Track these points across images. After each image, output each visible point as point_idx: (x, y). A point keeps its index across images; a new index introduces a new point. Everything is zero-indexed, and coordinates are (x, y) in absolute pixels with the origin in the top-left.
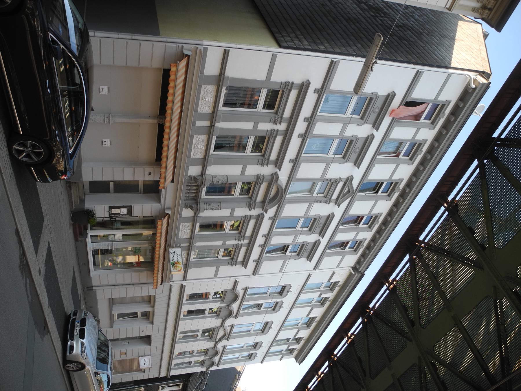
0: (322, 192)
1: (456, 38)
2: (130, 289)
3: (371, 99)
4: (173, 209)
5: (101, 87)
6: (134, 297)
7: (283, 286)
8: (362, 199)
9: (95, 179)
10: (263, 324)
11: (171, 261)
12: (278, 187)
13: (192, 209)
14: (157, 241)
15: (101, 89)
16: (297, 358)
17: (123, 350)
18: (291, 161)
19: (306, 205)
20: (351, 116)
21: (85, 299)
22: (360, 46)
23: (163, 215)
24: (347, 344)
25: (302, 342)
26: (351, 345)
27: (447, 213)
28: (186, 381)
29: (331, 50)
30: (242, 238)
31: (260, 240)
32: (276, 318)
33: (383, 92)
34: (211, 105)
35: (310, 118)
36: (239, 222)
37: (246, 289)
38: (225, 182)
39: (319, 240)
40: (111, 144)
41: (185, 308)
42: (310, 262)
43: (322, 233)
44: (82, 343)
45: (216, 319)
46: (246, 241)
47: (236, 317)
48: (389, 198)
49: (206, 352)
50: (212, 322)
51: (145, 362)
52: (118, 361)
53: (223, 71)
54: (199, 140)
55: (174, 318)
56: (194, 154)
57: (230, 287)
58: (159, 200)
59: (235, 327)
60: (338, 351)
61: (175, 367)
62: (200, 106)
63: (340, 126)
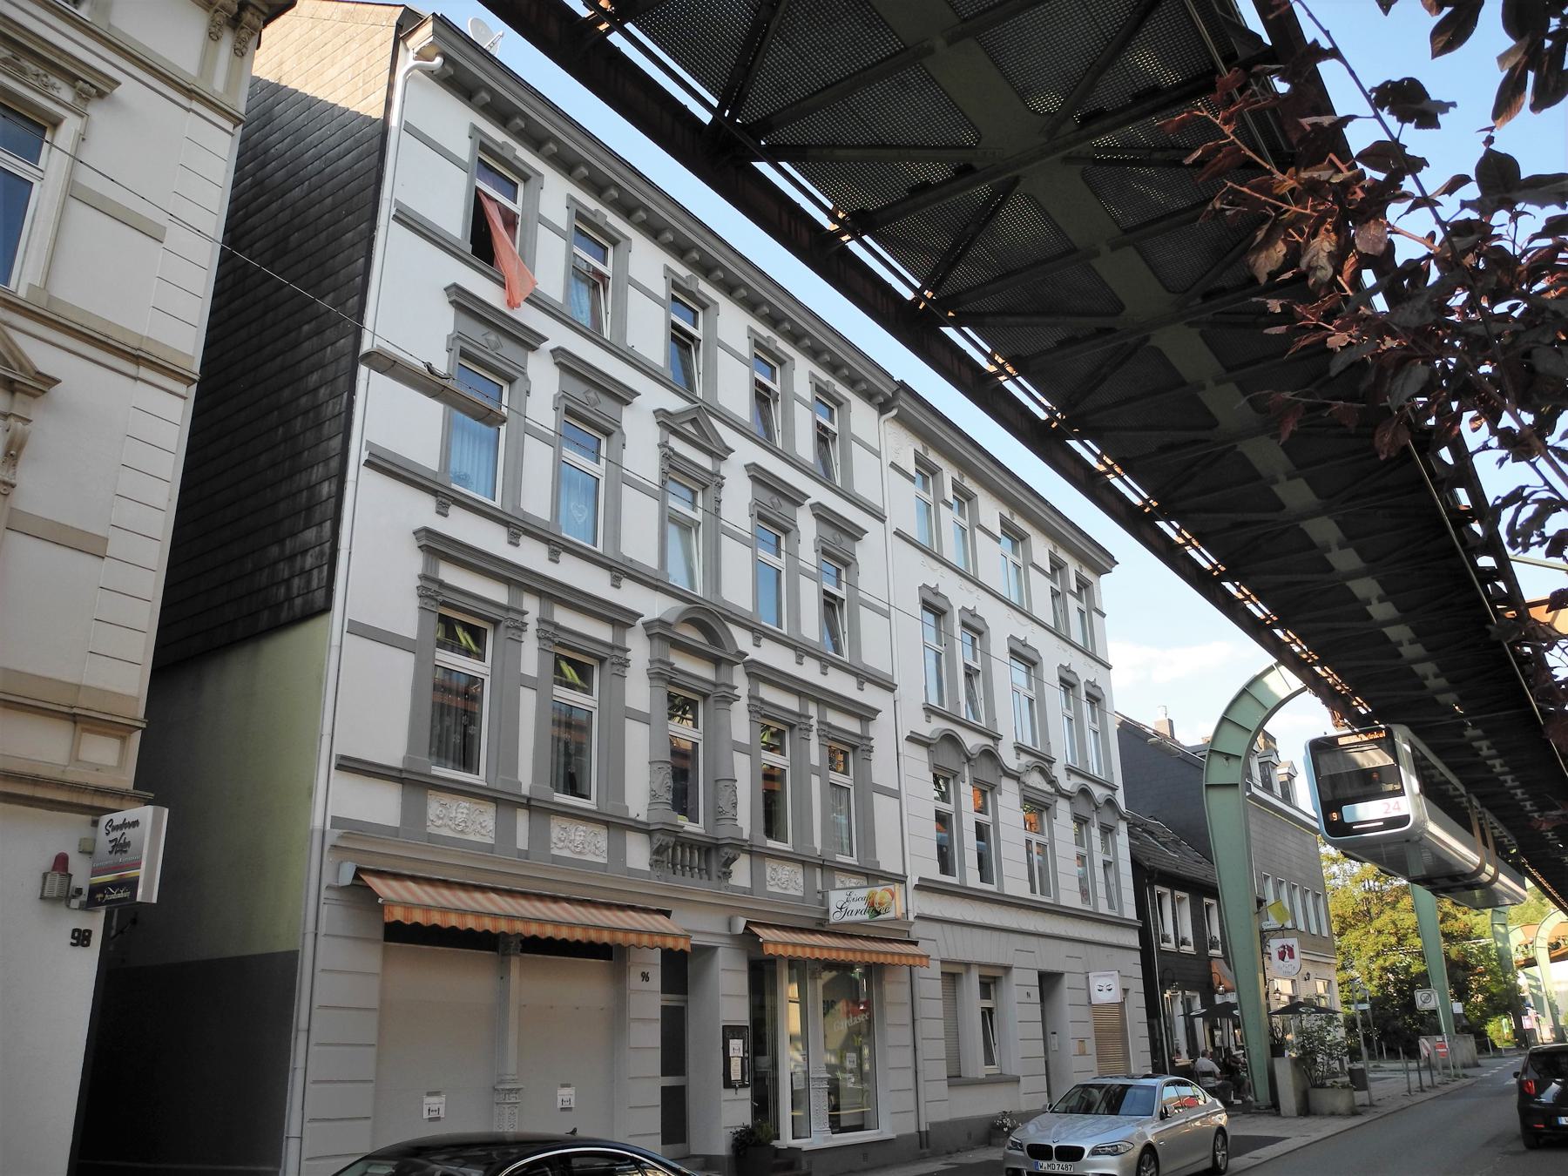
0: (689, 496)
1: (272, 80)
2: (925, 1028)
3: (464, 354)
4: (731, 911)
5: (426, 1115)
6: (945, 1019)
7: (924, 608)
8: (711, 384)
9: (657, 1127)
10: (1014, 663)
11: (867, 917)
12: (683, 622)
13: (735, 859)
14: (813, 955)
15: (433, 1115)
16: (1100, 571)
17: (1073, 1047)
18: (554, 558)
19: (726, 541)
20: (700, 511)
21: (949, 1153)
22: (315, 377)
23: (749, 940)
24: (1020, 379)
25: (1062, 555)
26: (1023, 366)
27: (629, 26)
28: (1149, 878)
29: (334, 463)
30: (865, 742)
31: (809, 672)
32: (1002, 626)
33: (446, 320)
34: (477, 806)
35: (512, 529)
36: (564, 665)
37: (930, 711)
38: (668, 769)
39: (811, 506)
40: (568, 1086)
41: (973, 880)
42: (639, 394)
43: (795, 498)
44: (1095, 1152)
45: (1000, 794)
46: (813, 710)
47: (996, 738)
48: (532, 180)
49: (1081, 821)
50: (1009, 799)
51: (1105, 989)
52: (1099, 1061)
53: (394, 774)
54: (442, 819)
55: (996, 908)
56: (484, 833)
57: (921, 754)
58: (706, 952)
59: (1020, 740)
60: (1132, 493)
61: (1117, 908)
62: (477, 838)
63: (530, 443)
